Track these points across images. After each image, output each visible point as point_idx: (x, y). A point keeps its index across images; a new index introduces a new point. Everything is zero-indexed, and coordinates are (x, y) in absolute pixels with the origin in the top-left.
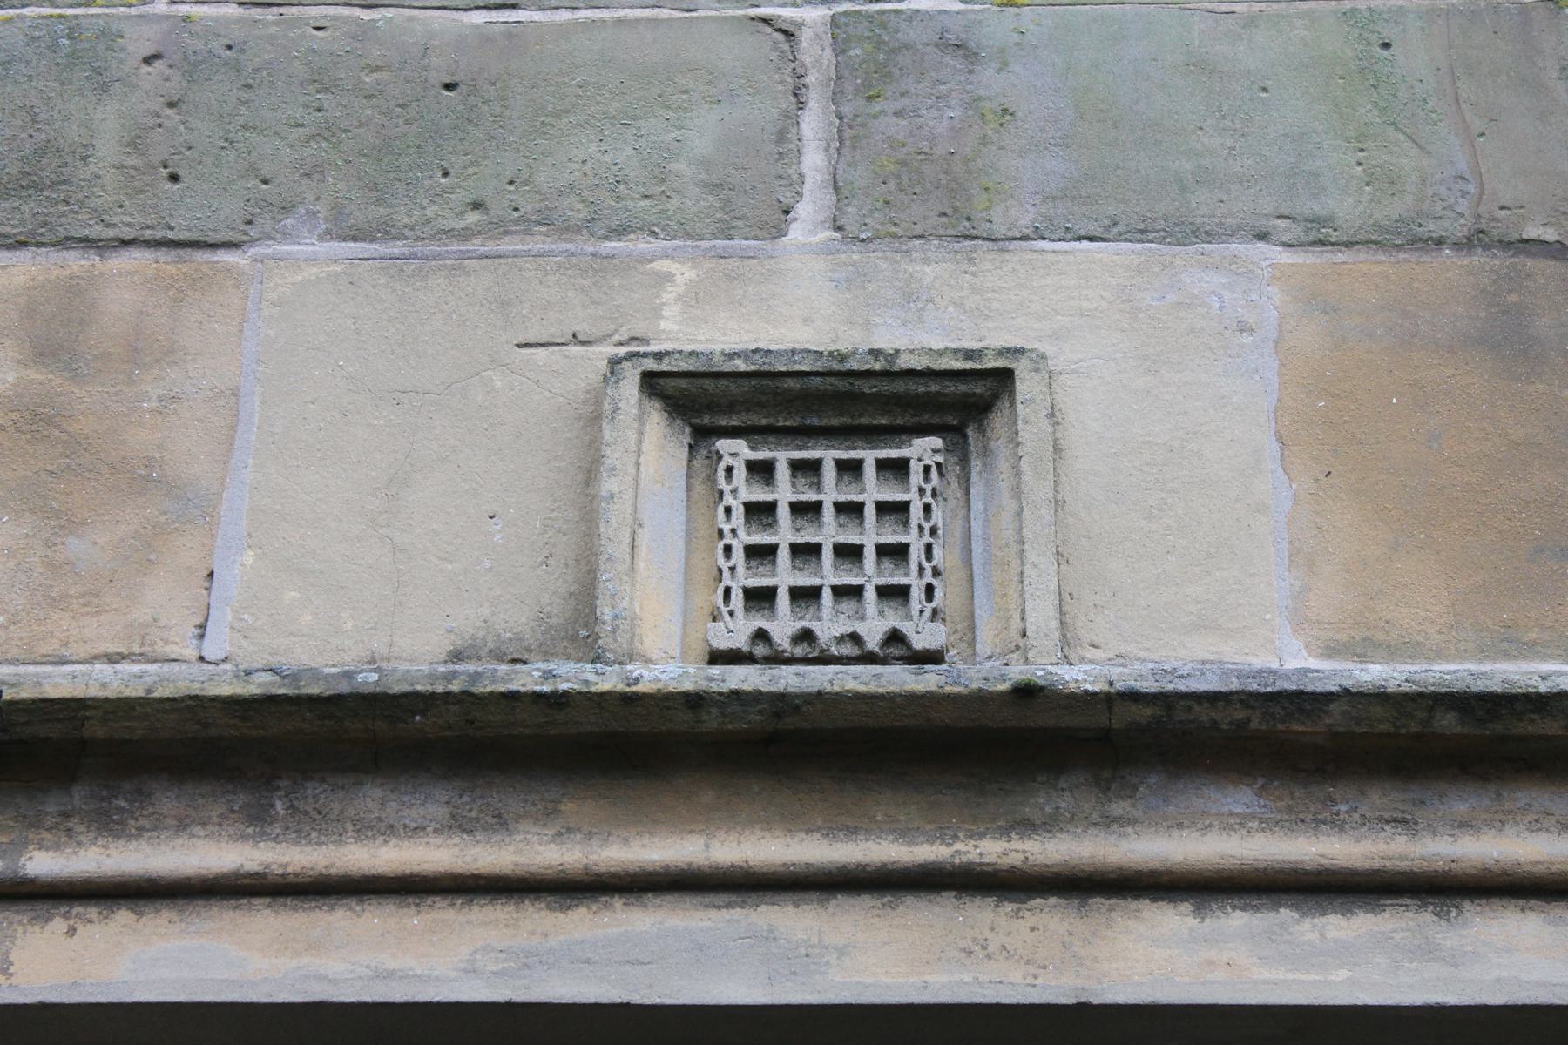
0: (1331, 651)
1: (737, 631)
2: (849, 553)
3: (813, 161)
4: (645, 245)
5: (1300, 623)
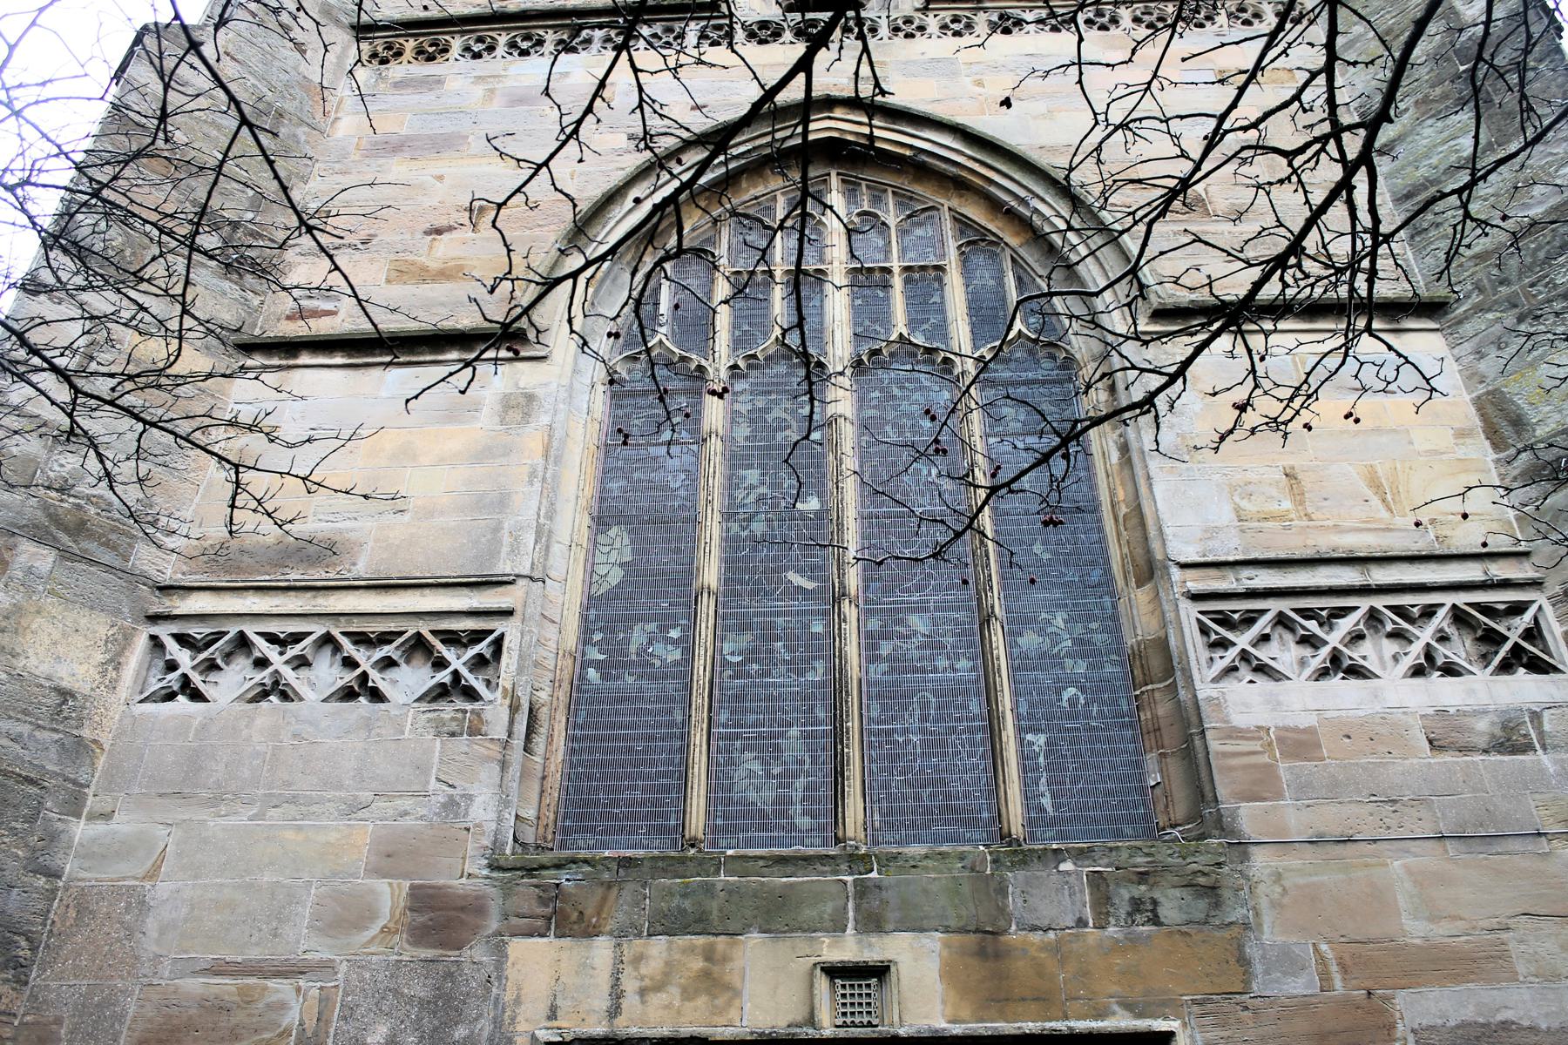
0: (949, 1022)
1: (839, 1021)
2: (860, 1004)
3: (851, 914)
4: (820, 934)
5: (943, 1016)
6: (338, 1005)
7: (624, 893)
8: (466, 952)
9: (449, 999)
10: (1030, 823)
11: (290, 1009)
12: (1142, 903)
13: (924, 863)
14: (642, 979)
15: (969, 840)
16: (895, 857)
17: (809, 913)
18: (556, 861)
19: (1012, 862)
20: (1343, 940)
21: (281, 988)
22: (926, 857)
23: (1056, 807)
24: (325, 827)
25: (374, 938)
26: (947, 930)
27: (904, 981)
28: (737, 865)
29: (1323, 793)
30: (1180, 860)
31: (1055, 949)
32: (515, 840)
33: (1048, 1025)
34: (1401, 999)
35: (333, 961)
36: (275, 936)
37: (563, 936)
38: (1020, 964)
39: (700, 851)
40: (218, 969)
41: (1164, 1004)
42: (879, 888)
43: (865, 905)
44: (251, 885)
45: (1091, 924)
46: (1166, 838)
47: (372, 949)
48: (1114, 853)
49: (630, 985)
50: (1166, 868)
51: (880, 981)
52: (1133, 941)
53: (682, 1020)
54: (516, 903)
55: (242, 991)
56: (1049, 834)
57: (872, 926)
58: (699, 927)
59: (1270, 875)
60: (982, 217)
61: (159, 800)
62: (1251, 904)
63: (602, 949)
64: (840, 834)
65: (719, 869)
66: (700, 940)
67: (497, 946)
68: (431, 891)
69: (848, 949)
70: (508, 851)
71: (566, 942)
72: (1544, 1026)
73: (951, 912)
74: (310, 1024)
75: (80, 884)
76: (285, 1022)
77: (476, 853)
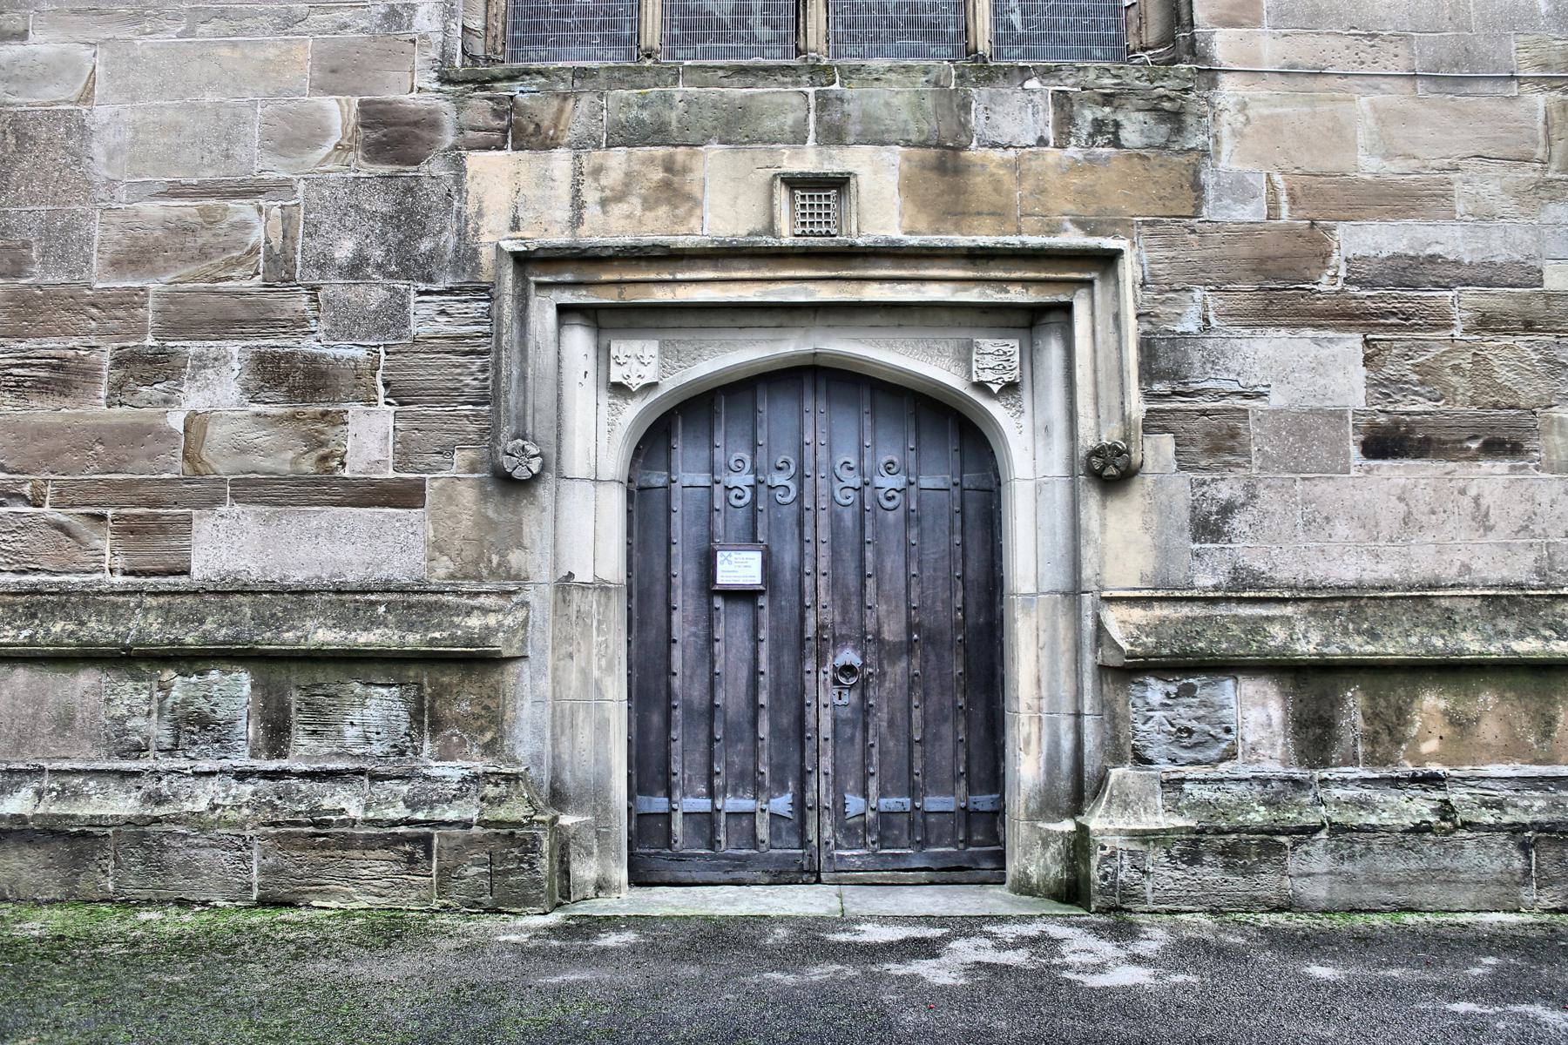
1: (799, 231)
3: (812, 126)
4: (780, 146)
6: (302, 223)
7: (580, 105)
8: (424, 168)
9: (411, 213)
10: (998, 39)
11: (254, 227)
12: (1106, 125)
13: (888, 76)
14: (603, 190)
15: (934, 56)
16: (858, 69)
17: (769, 125)
18: (508, 73)
19: (977, 78)
20: (1297, 171)
21: (243, 209)
22: (890, 70)
23: (1026, 24)
24: (262, 43)
25: (329, 155)
26: (908, 144)
27: (863, 193)
28: (696, 76)
29: (1303, 22)
30: (1147, 84)
31: (1015, 166)
32: (464, 52)
33: (1002, 239)
34: (1342, 231)
35: (288, 180)
36: (228, 157)
37: (521, 148)
38: (979, 179)
39: (657, 62)
40: (176, 191)
41: (1115, 223)
42: (841, 100)
43: (827, 118)
44: (193, 107)
45: (1052, 144)
46: (1136, 61)
47: (328, 167)
48: (1081, 73)
49: (590, 196)
50: (1133, 91)
51: (839, 193)
52: (1092, 161)
53: (644, 228)
54: (468, 116)
55: (203, 212)
56: (1016, 52)
57: (832, 138)
58: (657, 140)
59: (1235, 104)
60: (964, 269)
61: (74, 18)
62: (1213, 131)
63: (560, 162)
64: (802, 45)
65: (678, 79)
66: (660, 151)
67: (455, 160)
68: (380, 106)
69: (808, 160)
70: (458, 64)
71: (525, 154)
72: (1467, 261)
73: (912, 126)
74: (277, 242)
75: (11, 109)
76: (252, 241)
77: (424, 66)
